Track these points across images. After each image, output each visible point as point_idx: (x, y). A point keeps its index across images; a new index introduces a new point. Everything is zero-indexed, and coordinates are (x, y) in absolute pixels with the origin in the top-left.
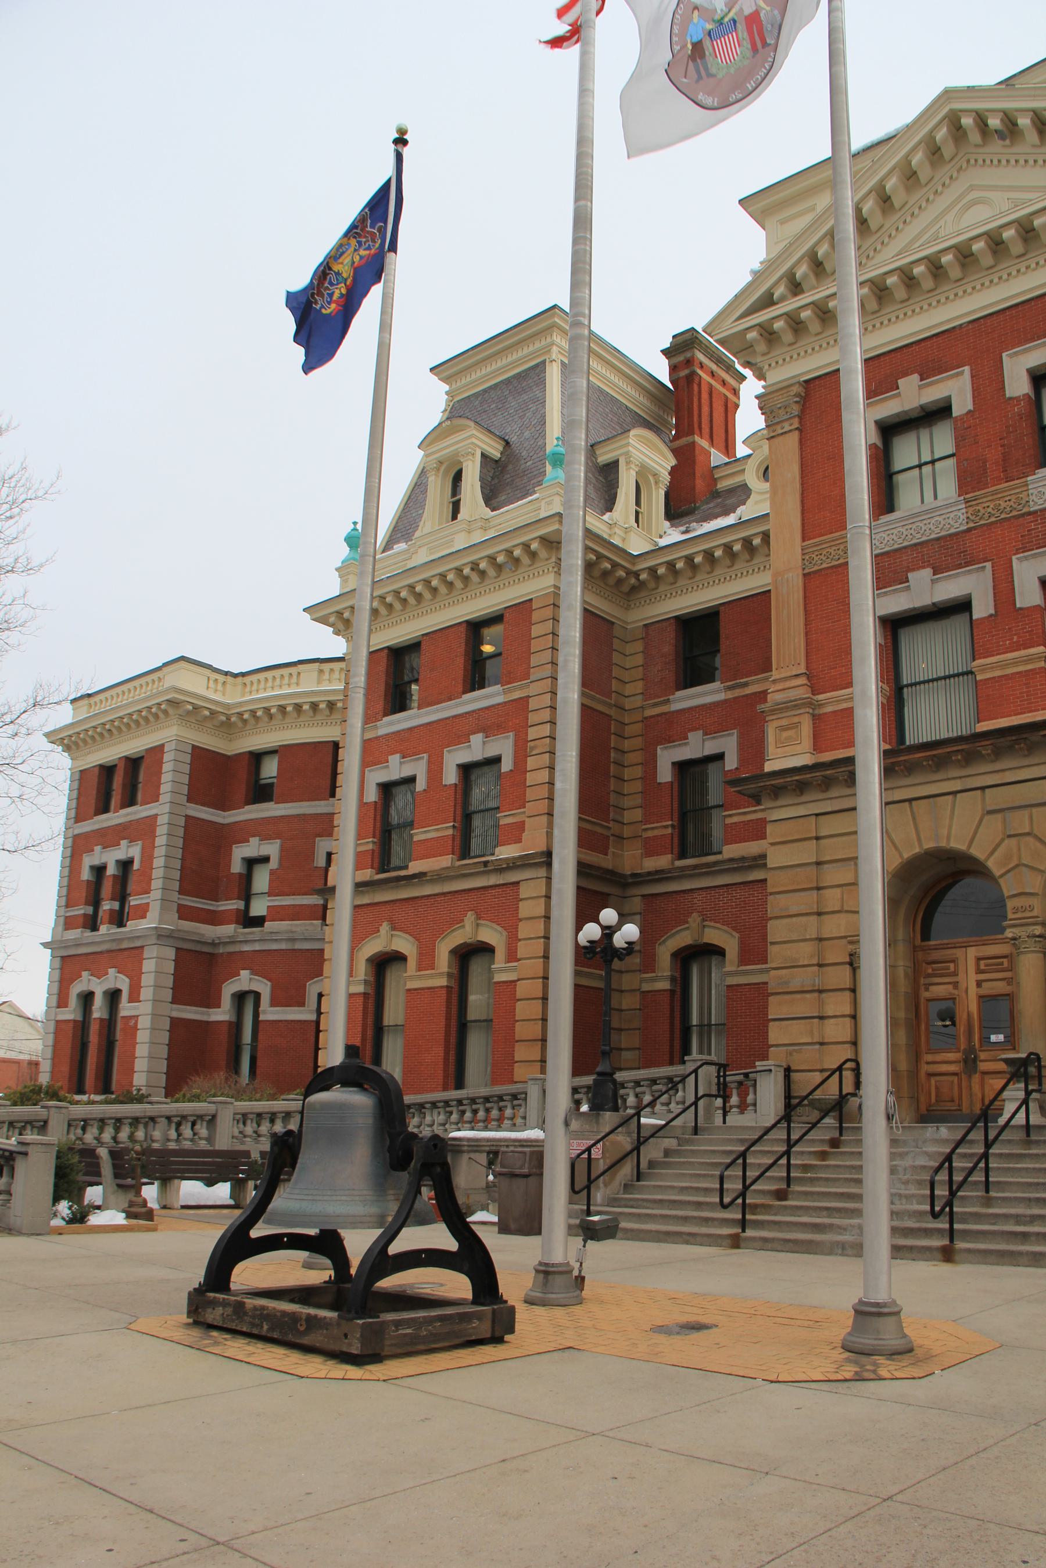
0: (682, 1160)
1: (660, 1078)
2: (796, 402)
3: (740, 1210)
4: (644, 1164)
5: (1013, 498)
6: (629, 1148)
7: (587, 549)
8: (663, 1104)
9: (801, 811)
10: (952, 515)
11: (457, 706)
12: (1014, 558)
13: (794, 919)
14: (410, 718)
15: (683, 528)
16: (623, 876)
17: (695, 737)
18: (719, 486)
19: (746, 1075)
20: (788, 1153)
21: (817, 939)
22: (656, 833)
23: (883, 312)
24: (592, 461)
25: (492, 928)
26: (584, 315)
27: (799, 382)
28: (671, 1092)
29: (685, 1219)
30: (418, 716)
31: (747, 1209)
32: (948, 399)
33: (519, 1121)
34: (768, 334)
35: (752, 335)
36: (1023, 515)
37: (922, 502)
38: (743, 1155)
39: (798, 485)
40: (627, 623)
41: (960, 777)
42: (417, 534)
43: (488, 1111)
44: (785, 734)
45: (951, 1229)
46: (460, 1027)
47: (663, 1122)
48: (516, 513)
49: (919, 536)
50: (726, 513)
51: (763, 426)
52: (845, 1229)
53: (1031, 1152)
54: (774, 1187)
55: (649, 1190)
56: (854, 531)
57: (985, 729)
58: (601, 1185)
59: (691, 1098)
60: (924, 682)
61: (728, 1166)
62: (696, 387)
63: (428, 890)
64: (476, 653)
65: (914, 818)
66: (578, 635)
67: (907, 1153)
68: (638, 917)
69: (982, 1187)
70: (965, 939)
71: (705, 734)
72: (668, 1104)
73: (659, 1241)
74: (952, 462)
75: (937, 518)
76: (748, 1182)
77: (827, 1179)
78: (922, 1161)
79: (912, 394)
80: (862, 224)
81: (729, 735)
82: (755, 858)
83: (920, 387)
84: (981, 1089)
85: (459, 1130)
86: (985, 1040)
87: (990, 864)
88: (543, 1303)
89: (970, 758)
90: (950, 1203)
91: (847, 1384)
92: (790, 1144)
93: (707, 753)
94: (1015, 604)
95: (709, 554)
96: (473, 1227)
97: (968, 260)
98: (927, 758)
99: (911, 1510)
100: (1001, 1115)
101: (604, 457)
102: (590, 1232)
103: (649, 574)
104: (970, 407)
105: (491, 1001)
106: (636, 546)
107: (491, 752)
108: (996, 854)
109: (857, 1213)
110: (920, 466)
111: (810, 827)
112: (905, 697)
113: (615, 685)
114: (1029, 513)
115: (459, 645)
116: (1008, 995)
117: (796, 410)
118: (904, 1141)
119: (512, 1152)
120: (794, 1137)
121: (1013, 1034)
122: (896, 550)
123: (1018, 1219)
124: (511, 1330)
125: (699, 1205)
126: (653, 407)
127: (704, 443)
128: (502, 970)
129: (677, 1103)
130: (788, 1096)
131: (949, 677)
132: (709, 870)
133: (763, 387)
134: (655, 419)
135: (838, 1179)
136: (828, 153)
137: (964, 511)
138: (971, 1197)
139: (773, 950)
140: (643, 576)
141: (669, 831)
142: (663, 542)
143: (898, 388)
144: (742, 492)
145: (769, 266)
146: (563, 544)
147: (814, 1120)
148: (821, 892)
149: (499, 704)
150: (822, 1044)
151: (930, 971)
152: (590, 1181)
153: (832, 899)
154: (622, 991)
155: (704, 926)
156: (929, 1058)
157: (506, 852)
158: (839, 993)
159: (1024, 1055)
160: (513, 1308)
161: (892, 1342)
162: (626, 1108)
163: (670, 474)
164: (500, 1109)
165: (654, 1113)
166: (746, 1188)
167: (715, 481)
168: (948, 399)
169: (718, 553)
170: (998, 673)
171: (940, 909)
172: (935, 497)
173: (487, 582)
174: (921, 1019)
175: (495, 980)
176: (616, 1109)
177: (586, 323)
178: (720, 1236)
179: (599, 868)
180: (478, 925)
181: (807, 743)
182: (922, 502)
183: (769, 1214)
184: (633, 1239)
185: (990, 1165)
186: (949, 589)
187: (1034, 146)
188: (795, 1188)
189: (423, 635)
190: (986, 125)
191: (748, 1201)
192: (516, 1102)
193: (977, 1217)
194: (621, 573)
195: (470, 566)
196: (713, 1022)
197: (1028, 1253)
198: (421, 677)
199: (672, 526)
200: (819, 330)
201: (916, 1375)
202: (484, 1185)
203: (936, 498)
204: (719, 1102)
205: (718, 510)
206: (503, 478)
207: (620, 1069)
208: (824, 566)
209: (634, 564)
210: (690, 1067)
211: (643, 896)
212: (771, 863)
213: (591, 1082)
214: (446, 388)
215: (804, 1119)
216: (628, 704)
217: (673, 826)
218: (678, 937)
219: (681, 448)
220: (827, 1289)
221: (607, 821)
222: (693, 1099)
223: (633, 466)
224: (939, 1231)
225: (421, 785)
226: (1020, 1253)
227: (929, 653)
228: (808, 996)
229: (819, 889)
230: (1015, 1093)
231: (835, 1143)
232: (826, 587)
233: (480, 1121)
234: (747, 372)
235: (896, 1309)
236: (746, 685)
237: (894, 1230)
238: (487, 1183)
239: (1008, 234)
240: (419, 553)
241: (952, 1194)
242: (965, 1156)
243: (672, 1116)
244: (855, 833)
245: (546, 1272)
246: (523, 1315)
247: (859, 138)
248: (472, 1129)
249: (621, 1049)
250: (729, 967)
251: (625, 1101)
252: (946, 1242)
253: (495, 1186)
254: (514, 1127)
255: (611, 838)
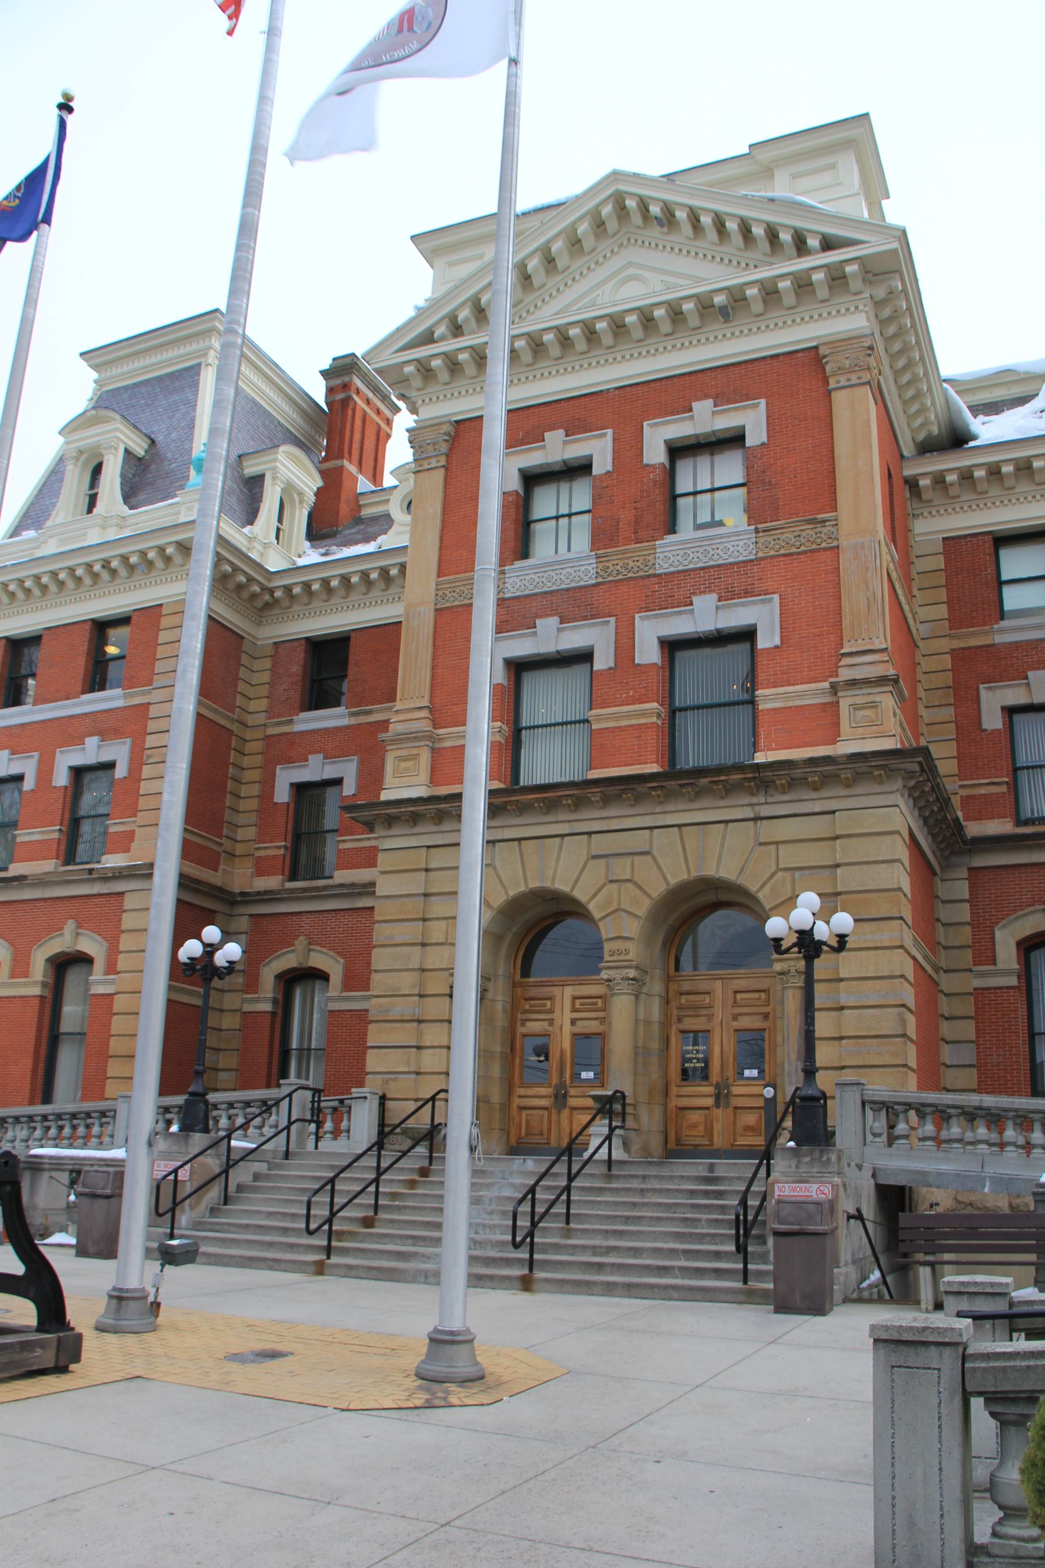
0: (271, 1184)
1: (254, 1101)
2: (446, 441)
3: (326, 1236)
4: (232, 1188)
5: (641, 559)
6: (217, 1170)
7: (219, 559)
8: (255, 1127)
9: (413, 842)
10: (583, 569)
11: (75, 705)
12: (637, 616)
13: (399, 949)
14: (24, 714)
15: (323, 551)
16: (232, 894)
17: (315, 760)
18: (363, 513)
19: (341, 1101)
20: (376, 1181)
21: (419, 969)
22: (269, 852)
23: (536, 367)
24: (238, 472)
25: (93, 938)
26: (239, 324)
27: (450, 422)
28: (265, 1115)
29: (271, 1245)
30: (32, 712)
31: (333, 1236)
32: (590, 458)
33: (106, 1139)
34: (425, 370)
35: (409, 369)
36: (649, 576)
37: (556, 552)
38: (332, 1181)
39: (438, 522)
40: (257, 639)
41: (569, 821)
42: (49, 523)
43: (74, 1127)
44: (403, 765)
45: (531, 1259)
46: (51, 1039)
47: (254, 1146)
48: (153, 515)
49: (549, 584)
50: (367, 540)
51: (411, 459)
52: (429, 1258)
53: (611, 1186)
54: (361, 1214)
55: (238, 1214)
56: (482, 572)
57: (596, 777)
58: (187, 1208)
59: (284, 1123)
60: (542, 726)
61: (316, 1192)
62: (350, 412)
63: (28, 894)
64: (100, 653)
65: (522, 857)
66: (199, 646)
67: (493, 1184)
68: (243, 937)
69: (564, 1218)
70: (563, 978)
71: (326, 757)
72: (260, 1127)
73: (243, 1266)
74: (587, 517)
75: (551, 573)
76: (335, 1209)
77: (414, 1208)
78: (507, 1192)
79: (556, 448)
80: (526, 279)
81: (349, 761)
82: (365, 886)
83: (565, 443)
84: (565, 1125)
85: (42, 1146)
86: (575, 1076)
87: (591, 907)
88: (115, 1330)
89: (579, 803)
90: (531, 1234)
91: (416, 1411)
92: (380, 1172)
93: (326, 776)
94: (634, 660)
95: (345, 579)
96: (42, 1249)
97: (620, 330)
98: (537, 800)
99: (467, 1535)
100: (587, 1149)
101: (251, 469)
102: (169, 1257)
103: (284, 592)
104: (610, 468)
105: (87, 1013)
106: (274, 562)
107: (105, 757)
108: (598, 898)
109: (438, 1241)
110: (557, 518)
111: (420, 859)
112: (523, 738)
113: (239, 701)
114: (655, 575)
115: (82, 644)
116: (600, 1034)
117: (444, 448)
118: (492, 1173)
119: (95, 1171)
120: (384, 1164)
121: (603, 1072)
122: (527, 596)
123: (595, 1250)
124: (77, 1359)
125: (285, 1231)
126: (308, 429)
127: (352, 468)
128: (99, 981)
129: (271, 1127)
130: (382, 1124)
131: (566, 723)
132: (318, 894)
133: (415, 422)
134: (304, 436)
135: (425, 1208)
136: (495, 210)
137: (594, 566)
138: (552, 1228)
139: (375, 978)
140: (278, 594)
141: (282, 851)
142: (301, 562)
143: (543, 440)
144: (385, 522)
145: (433, 304)
146: (194, 552)
147: (406, 1149)
148: (427, 923)
149: (117, 708)
150: (418, 1073)
151: (527, 1007)
152: (175, 1204)
153: (437, 931)
154: (222, 1011)
155: (310, 950)
156: (521, 1091)
157: (112, 861)
158: (438, 1024)
159: (610, 1093)
160: (79, 1338)
161: (466, 1370)
162: (218, 1130)
163: (316, 495)
164: (88, 1127)
165: (246, 1136)
166: (333, 1214)
167: (360, 507)
168: (590, 458)
169: (355, 579)
170: (612, 724)
171: (541, 947)
172: (565, 548)
173: (118, 581)
174: (513, 1053)
175: (92, 992)
176: (206, 1130)
177: (241, 332)
178: (305, 1263)
179: (207, 884)
180: (78, 934)
181: (424, 776)
182: (556, 552)
183: (355, 1241)
184: (215, 1264)
185: (572, 1198)
186: (573, 639)
187: (688, 238)
188: (382, 1215)
189: (45, 629)
190: (648, 210)
191: (334, 1228)
192: (104, 1120)
193: (557, 1248)
194: (257, 589)
195: (101, 563)
196: (313, 1047)
197: (603, 1283)
198: (39, 672)
199: (312, 547)
200: (475, 374)
201: (485, 1402)
202: (64, 1205)
203: (569, 550)
204: (313, 1127)
205: (359, 537)
206: (144, 477)
207: (216, 1090)
208: (456, 603)
209: (269, 580)
210: (285, 1090)
211: (250, 915)
212: (379, 891)
213: (182, 1102)
214: (95, 375)
215: (397, 1147)
216: (251, 720)
217: (286, 847)
218: (283, 959)
219: (328, 470)
220: (405, 1315)
221: (220, 837)
222: (286, 1123)
223: (279, 482)
224: (520, 1261)
225: (28, 784)
226: (594, 1283)
227: (548, 699)
228: (407, 1025)
229: (425, 920)
230: (600, 1128)
231: (424, 1172)
232: (452, 623)
233: (79, 1137)
234: (401, 404)
235: (470, 1337)
236: (369, 712)
237: (472, 1260)
238: (68, 1203)
239: (659, 313)
240: (47, 545)
241: (534, 1224)
242: (548, 1188)
243: (264, 1139)
244: (457, 868)
245: (120, 1298)
246: (91, 1343)
247: (525, 200)
248: (56, 1146)
249: (218, 1070)
250: (332, 993)
251: (217, 1122)
252: (526, 1271)
253: (75, 1207)
254: (100, 1146)
255: (223, 855)
